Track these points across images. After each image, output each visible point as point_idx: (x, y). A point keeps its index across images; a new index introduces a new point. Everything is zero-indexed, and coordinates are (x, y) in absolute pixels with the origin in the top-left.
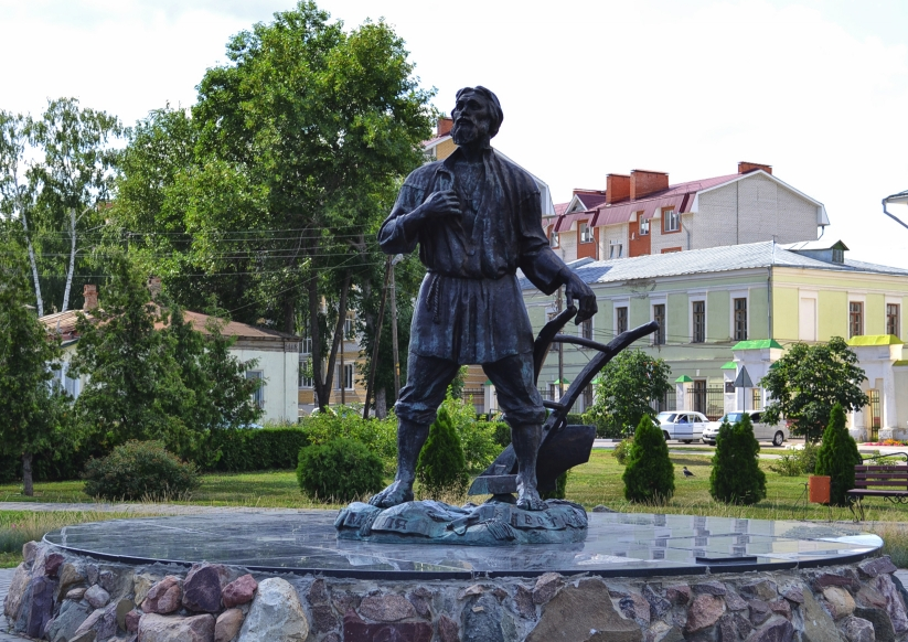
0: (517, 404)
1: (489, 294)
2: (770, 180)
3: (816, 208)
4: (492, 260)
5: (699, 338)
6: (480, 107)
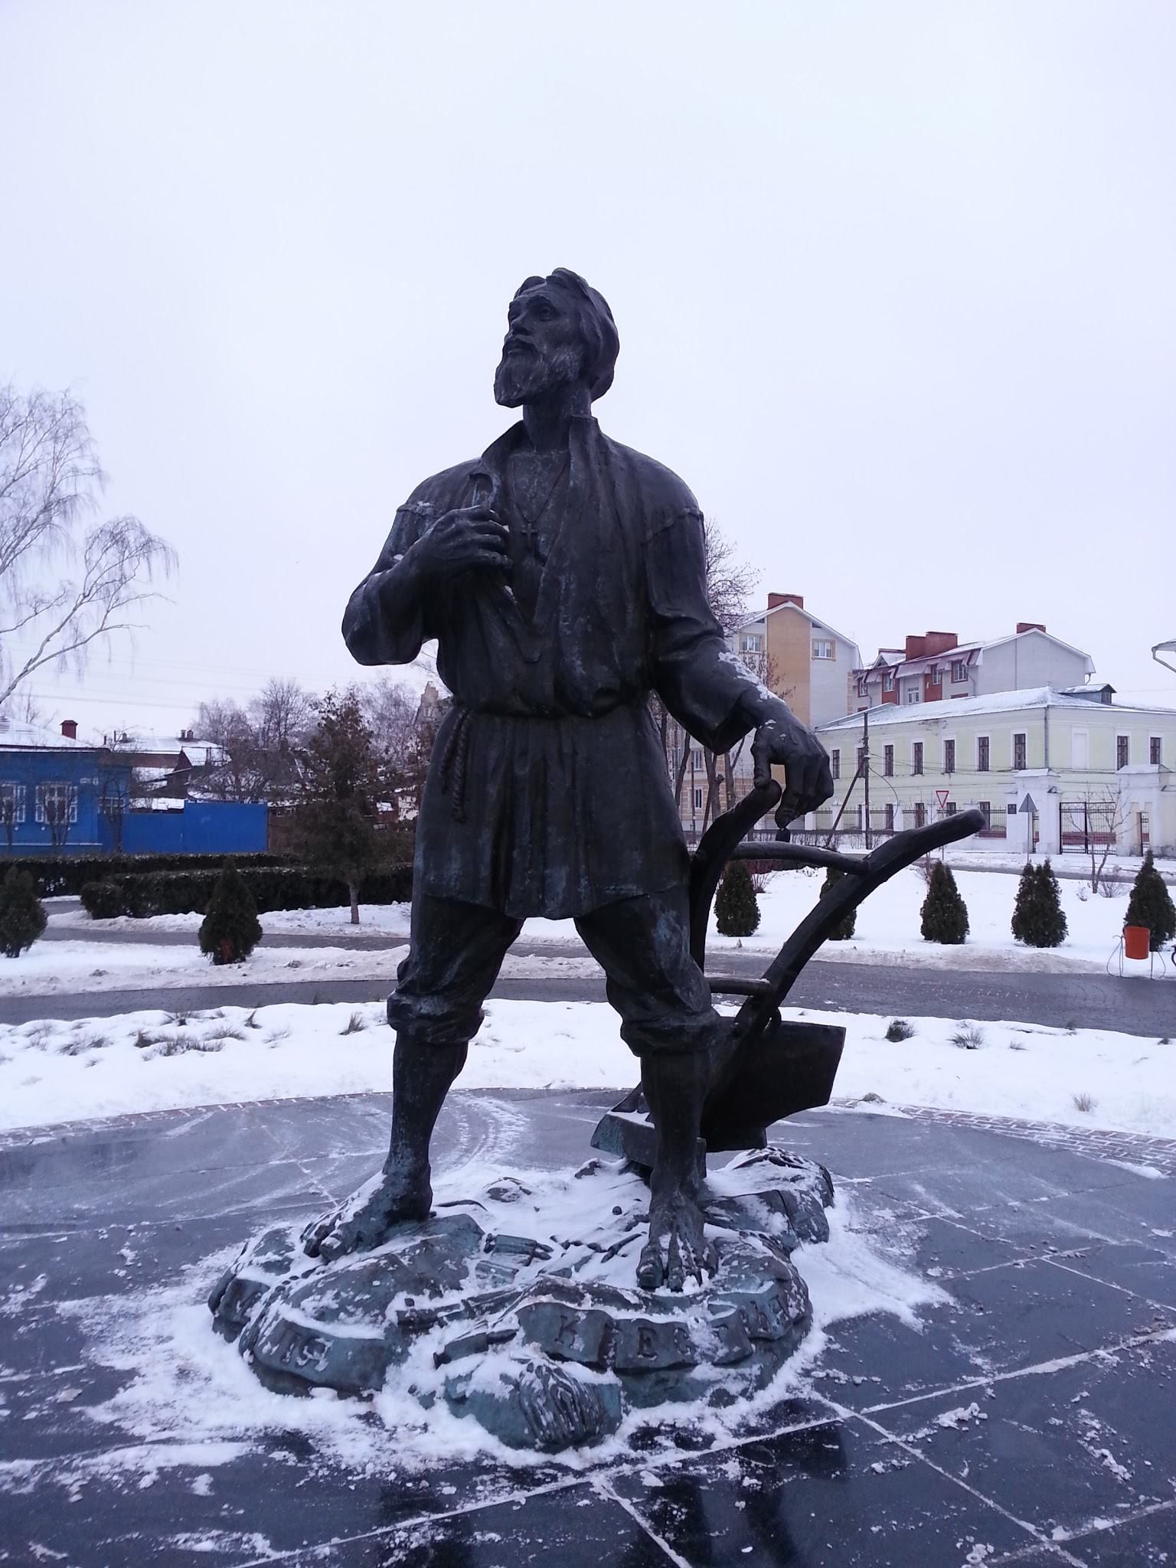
0: (645, 1006)
1: (575, 753)
2: (1044, 637)
3: (1083, 659)
4: (580, 670)
5: (984, 766)
6: (556, 314)
